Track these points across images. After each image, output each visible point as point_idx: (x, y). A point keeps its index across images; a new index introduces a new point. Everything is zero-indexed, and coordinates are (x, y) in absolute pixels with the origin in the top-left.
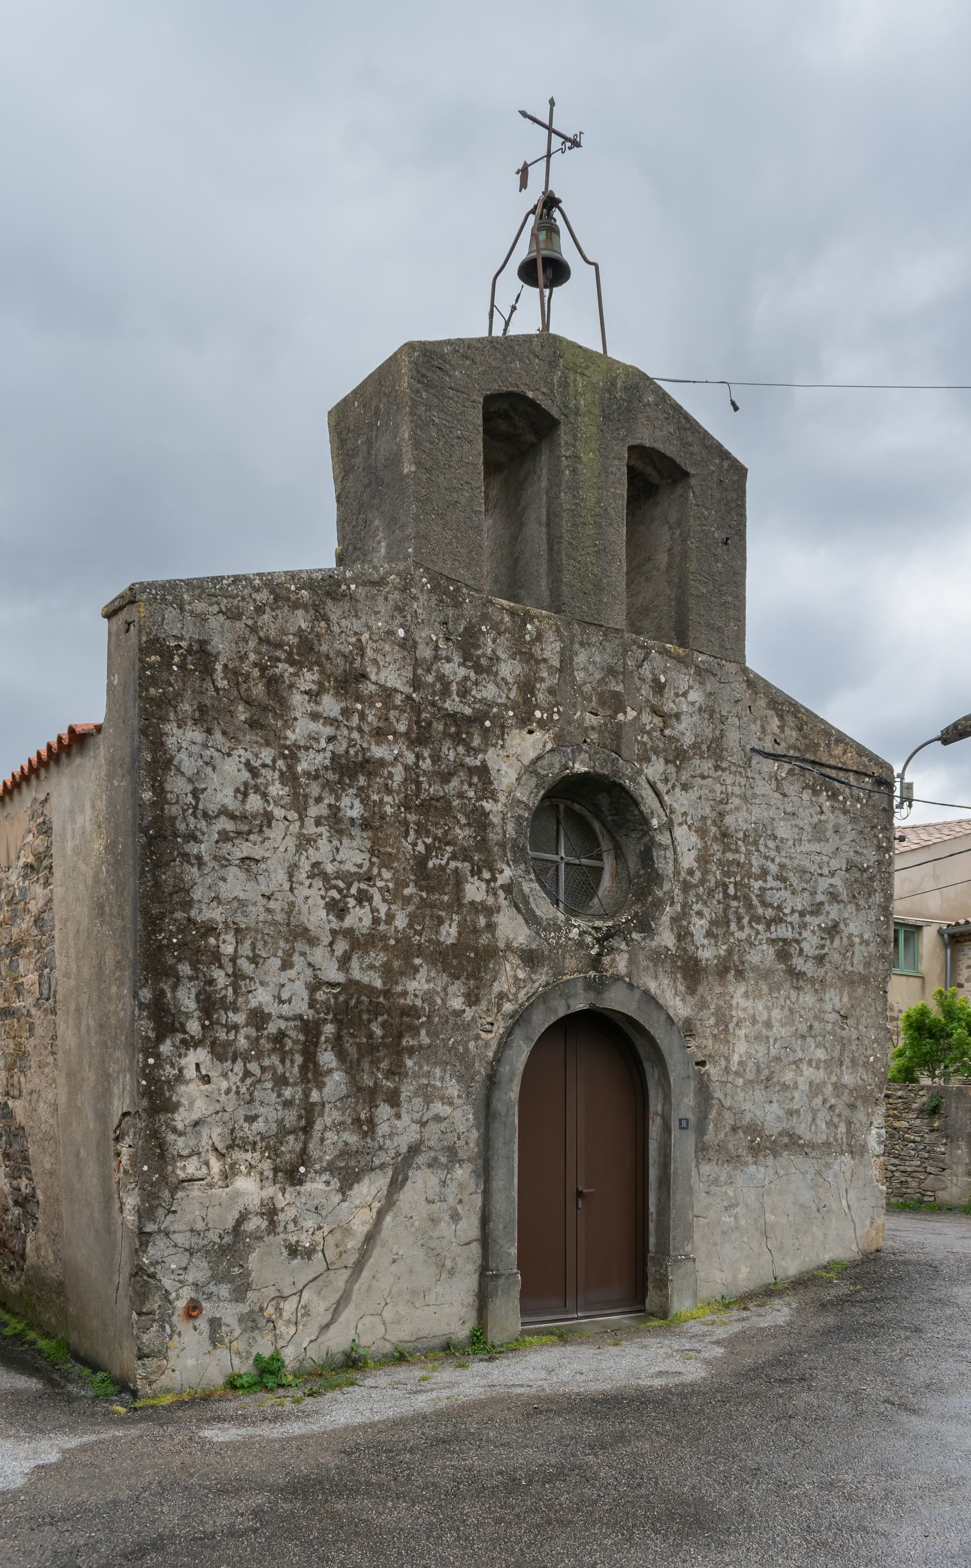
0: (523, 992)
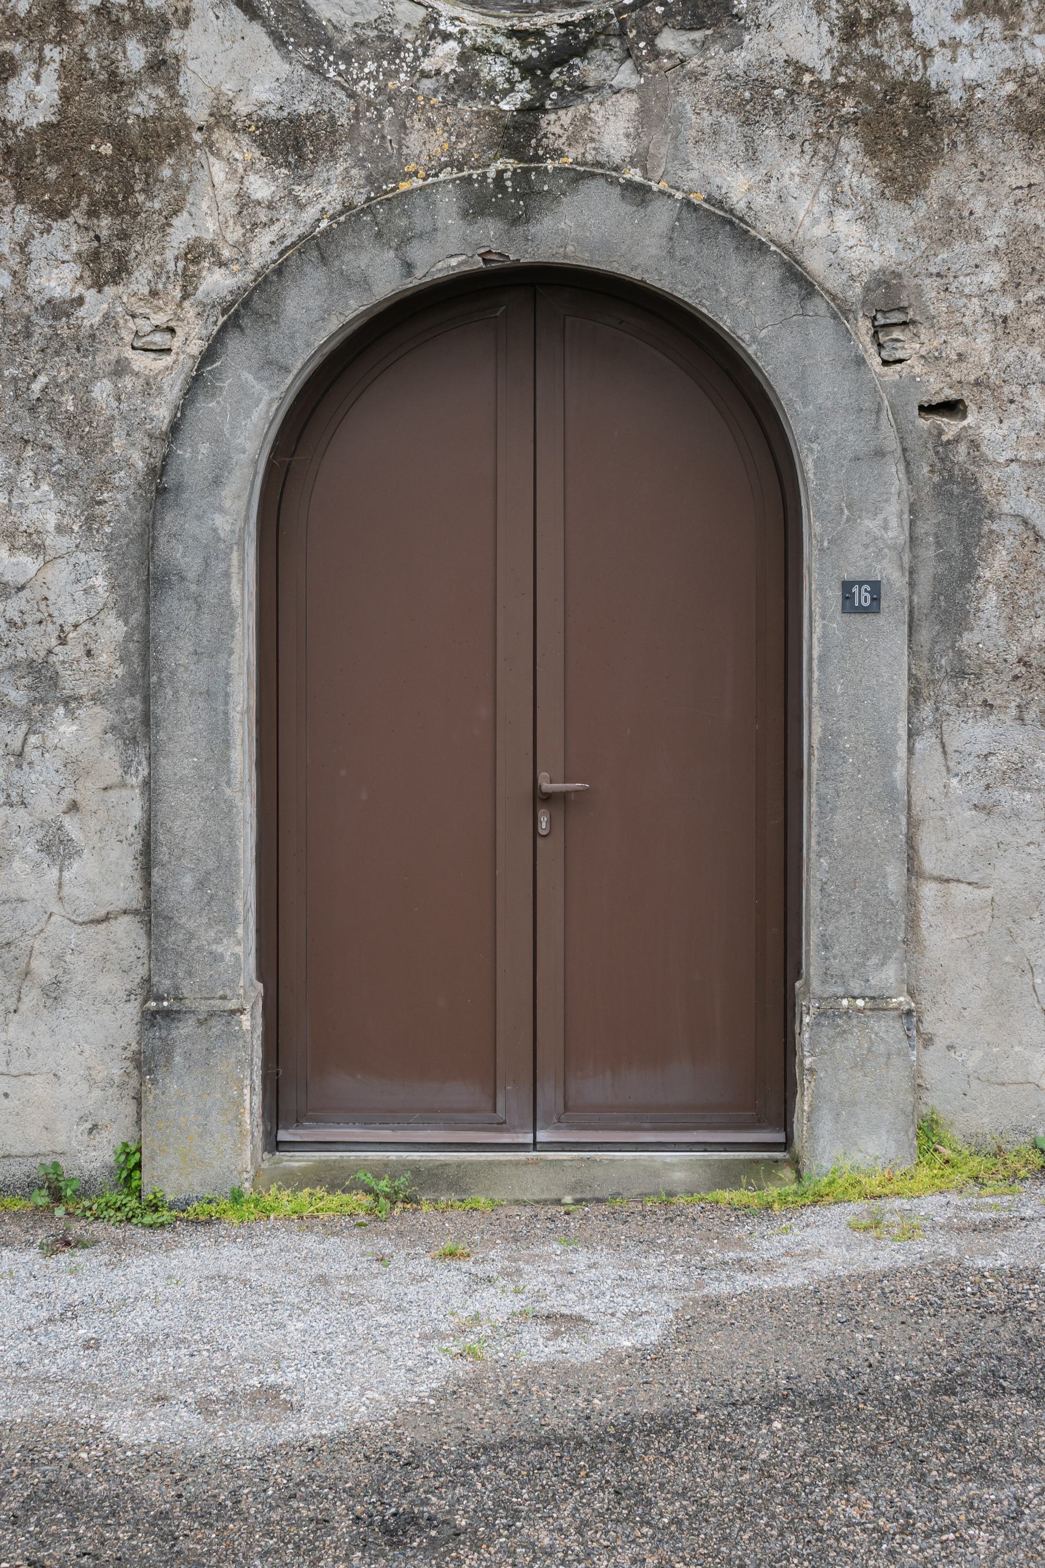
0: (265, 238)
